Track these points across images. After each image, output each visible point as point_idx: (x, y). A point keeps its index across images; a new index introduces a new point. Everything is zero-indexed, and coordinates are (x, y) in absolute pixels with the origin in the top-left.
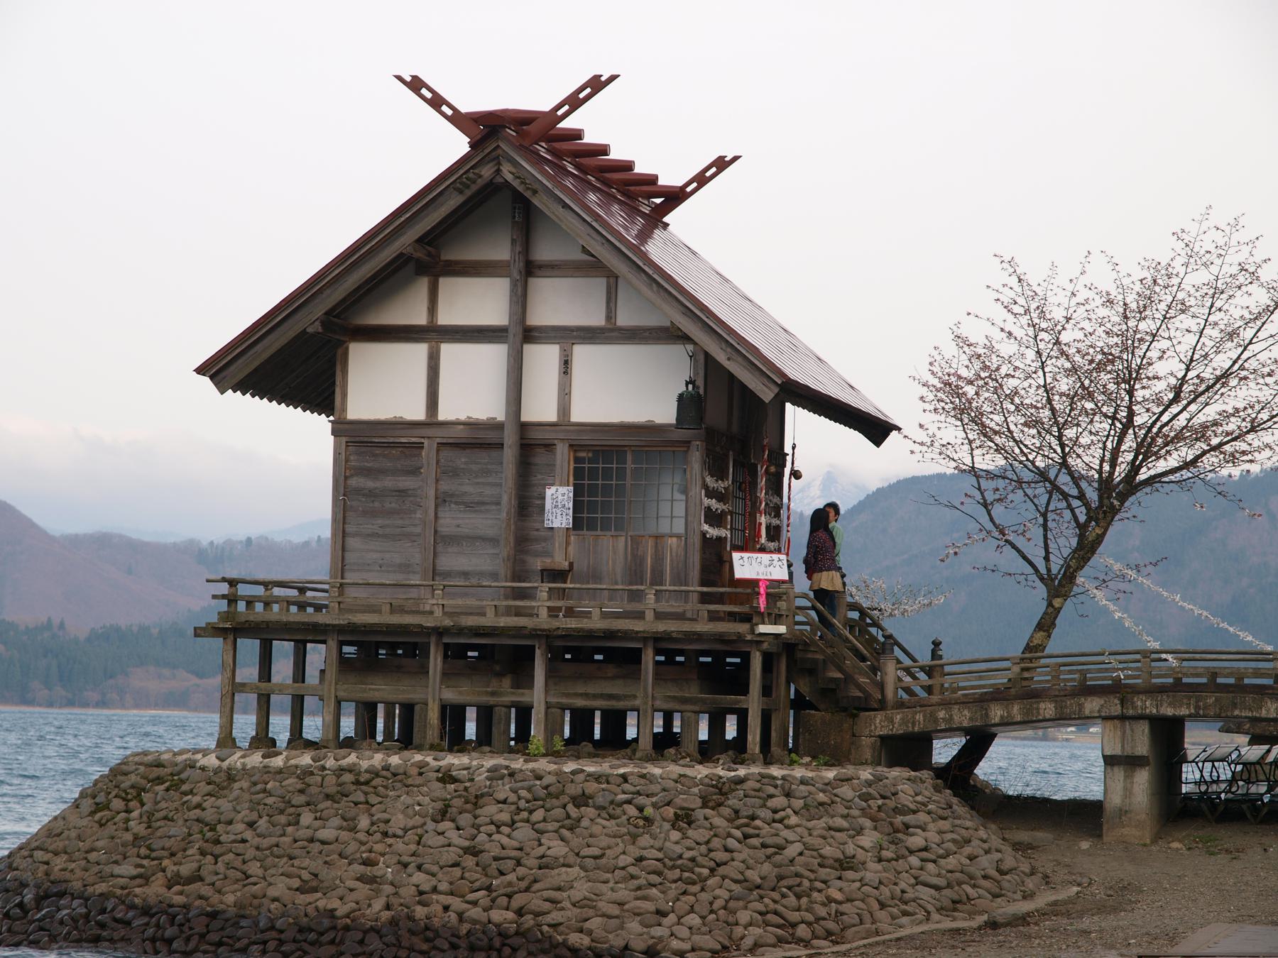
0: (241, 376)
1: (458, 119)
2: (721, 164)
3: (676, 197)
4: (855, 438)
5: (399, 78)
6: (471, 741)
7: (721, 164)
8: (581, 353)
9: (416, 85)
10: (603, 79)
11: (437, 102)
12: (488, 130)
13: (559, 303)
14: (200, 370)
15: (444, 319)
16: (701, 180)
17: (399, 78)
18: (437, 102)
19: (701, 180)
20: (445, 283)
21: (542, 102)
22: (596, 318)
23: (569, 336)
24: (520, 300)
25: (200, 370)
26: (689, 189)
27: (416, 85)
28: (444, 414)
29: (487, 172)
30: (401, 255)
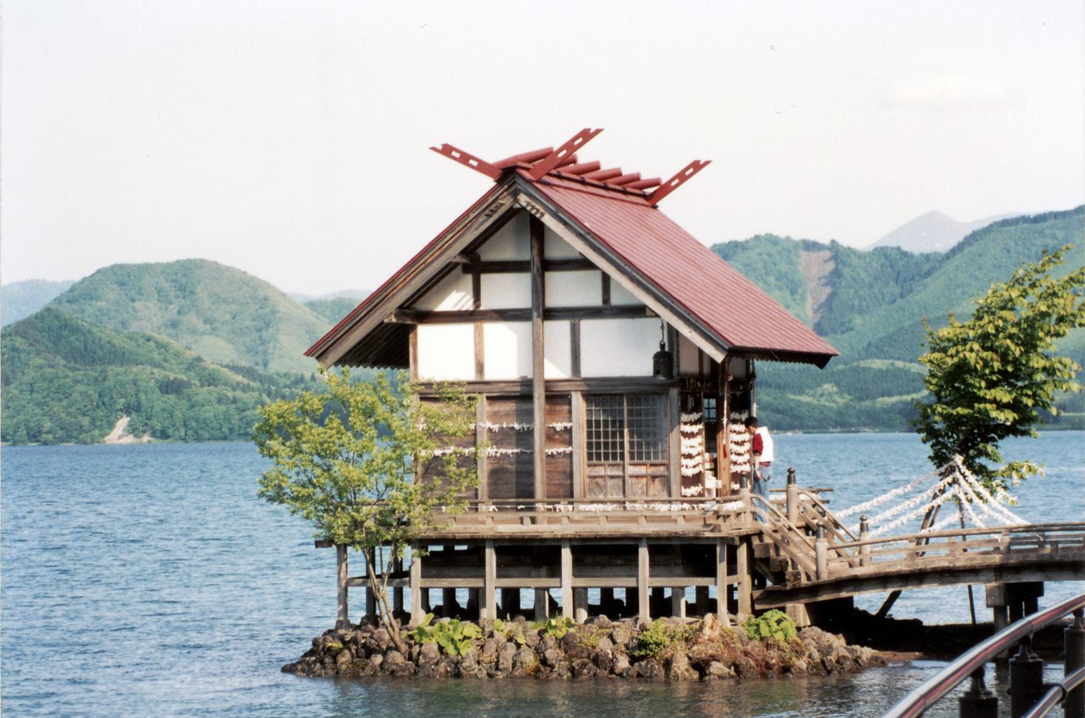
0: (336, 360)
1: (483, 167)
2: (697, 166)
3: (665, 189)
4: (813, 367)
5: (434, 149)
6: (724, 362)
7: (697, 166)
8: (586, 325)
9: (447, 150)
10: (592, 131)
11: (465, 159)
12: (507, 174)
13: (567, 289)
14: (308, 354)
15: (485, 305)
16: (682, 177)
17: (434, 149)
18: (465, 159)
19: (682, 177)
20: (485, 279)
21: (555, 140)
22: (596, 300)
23: (575, 314)
24: (539, 290)
25: (308, 354)
26: (673, 184)
27: (447, 150)
28: (488, 376)
29: (507, 202)
30: (450, 263)
